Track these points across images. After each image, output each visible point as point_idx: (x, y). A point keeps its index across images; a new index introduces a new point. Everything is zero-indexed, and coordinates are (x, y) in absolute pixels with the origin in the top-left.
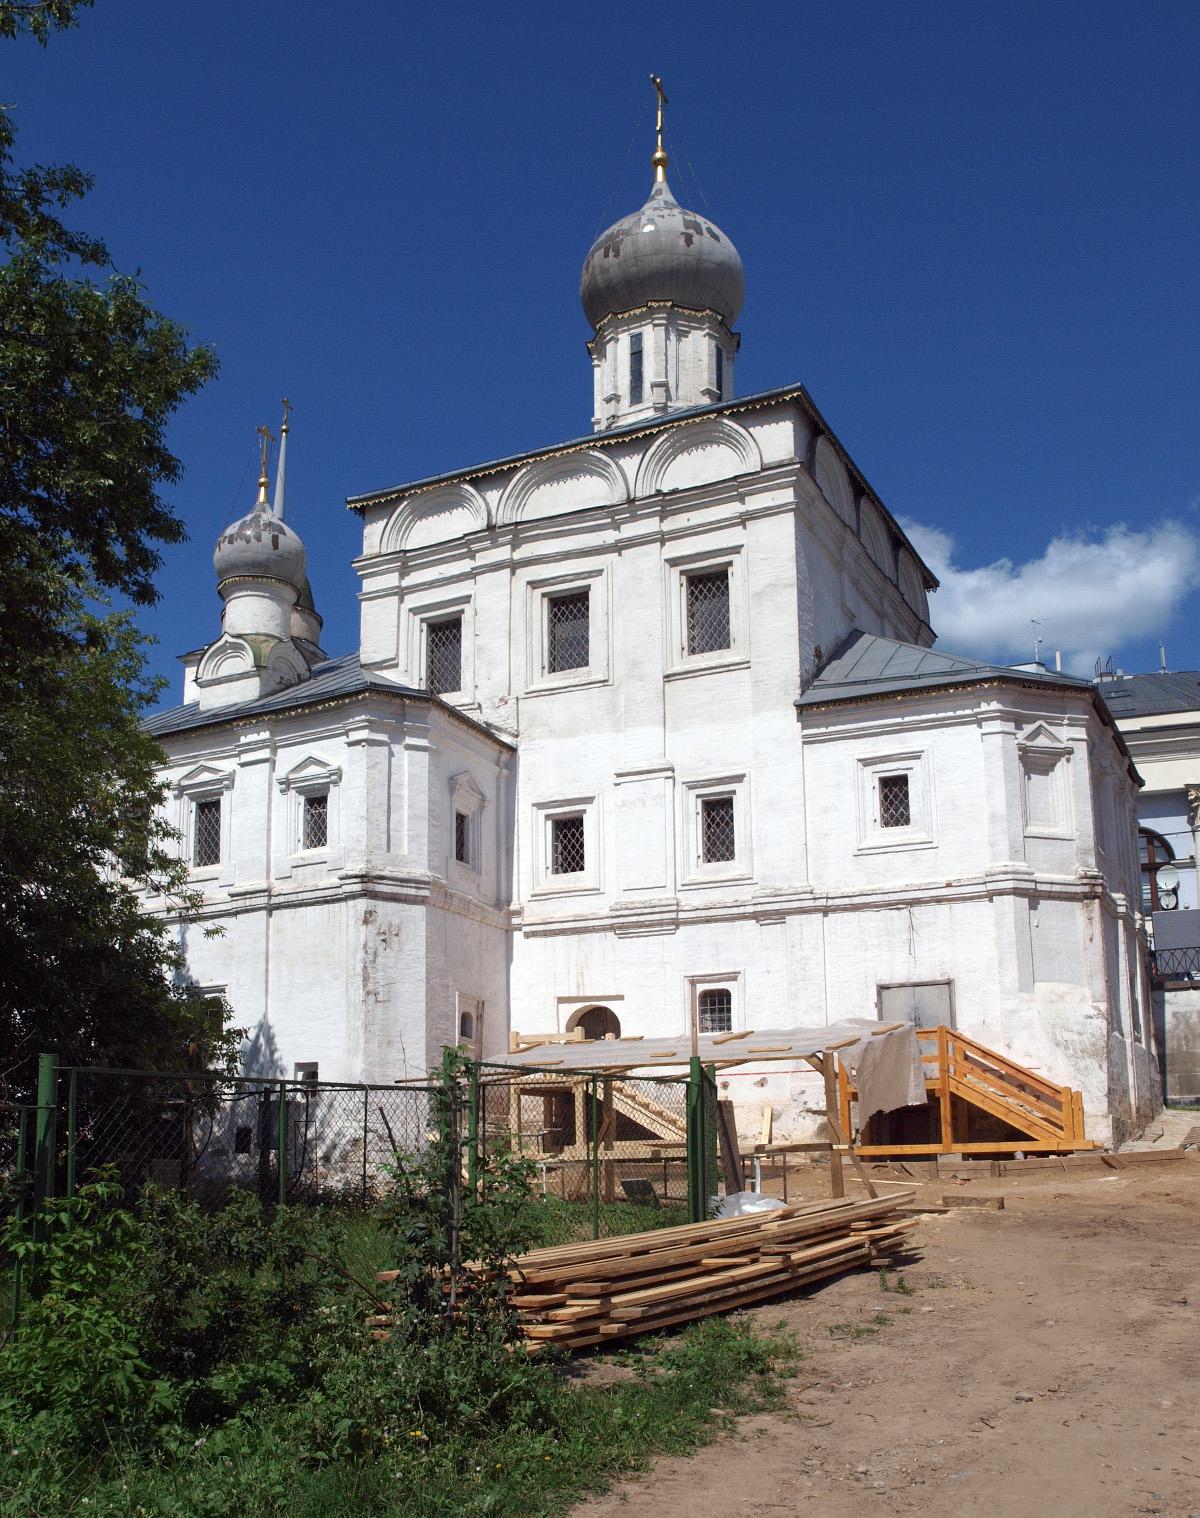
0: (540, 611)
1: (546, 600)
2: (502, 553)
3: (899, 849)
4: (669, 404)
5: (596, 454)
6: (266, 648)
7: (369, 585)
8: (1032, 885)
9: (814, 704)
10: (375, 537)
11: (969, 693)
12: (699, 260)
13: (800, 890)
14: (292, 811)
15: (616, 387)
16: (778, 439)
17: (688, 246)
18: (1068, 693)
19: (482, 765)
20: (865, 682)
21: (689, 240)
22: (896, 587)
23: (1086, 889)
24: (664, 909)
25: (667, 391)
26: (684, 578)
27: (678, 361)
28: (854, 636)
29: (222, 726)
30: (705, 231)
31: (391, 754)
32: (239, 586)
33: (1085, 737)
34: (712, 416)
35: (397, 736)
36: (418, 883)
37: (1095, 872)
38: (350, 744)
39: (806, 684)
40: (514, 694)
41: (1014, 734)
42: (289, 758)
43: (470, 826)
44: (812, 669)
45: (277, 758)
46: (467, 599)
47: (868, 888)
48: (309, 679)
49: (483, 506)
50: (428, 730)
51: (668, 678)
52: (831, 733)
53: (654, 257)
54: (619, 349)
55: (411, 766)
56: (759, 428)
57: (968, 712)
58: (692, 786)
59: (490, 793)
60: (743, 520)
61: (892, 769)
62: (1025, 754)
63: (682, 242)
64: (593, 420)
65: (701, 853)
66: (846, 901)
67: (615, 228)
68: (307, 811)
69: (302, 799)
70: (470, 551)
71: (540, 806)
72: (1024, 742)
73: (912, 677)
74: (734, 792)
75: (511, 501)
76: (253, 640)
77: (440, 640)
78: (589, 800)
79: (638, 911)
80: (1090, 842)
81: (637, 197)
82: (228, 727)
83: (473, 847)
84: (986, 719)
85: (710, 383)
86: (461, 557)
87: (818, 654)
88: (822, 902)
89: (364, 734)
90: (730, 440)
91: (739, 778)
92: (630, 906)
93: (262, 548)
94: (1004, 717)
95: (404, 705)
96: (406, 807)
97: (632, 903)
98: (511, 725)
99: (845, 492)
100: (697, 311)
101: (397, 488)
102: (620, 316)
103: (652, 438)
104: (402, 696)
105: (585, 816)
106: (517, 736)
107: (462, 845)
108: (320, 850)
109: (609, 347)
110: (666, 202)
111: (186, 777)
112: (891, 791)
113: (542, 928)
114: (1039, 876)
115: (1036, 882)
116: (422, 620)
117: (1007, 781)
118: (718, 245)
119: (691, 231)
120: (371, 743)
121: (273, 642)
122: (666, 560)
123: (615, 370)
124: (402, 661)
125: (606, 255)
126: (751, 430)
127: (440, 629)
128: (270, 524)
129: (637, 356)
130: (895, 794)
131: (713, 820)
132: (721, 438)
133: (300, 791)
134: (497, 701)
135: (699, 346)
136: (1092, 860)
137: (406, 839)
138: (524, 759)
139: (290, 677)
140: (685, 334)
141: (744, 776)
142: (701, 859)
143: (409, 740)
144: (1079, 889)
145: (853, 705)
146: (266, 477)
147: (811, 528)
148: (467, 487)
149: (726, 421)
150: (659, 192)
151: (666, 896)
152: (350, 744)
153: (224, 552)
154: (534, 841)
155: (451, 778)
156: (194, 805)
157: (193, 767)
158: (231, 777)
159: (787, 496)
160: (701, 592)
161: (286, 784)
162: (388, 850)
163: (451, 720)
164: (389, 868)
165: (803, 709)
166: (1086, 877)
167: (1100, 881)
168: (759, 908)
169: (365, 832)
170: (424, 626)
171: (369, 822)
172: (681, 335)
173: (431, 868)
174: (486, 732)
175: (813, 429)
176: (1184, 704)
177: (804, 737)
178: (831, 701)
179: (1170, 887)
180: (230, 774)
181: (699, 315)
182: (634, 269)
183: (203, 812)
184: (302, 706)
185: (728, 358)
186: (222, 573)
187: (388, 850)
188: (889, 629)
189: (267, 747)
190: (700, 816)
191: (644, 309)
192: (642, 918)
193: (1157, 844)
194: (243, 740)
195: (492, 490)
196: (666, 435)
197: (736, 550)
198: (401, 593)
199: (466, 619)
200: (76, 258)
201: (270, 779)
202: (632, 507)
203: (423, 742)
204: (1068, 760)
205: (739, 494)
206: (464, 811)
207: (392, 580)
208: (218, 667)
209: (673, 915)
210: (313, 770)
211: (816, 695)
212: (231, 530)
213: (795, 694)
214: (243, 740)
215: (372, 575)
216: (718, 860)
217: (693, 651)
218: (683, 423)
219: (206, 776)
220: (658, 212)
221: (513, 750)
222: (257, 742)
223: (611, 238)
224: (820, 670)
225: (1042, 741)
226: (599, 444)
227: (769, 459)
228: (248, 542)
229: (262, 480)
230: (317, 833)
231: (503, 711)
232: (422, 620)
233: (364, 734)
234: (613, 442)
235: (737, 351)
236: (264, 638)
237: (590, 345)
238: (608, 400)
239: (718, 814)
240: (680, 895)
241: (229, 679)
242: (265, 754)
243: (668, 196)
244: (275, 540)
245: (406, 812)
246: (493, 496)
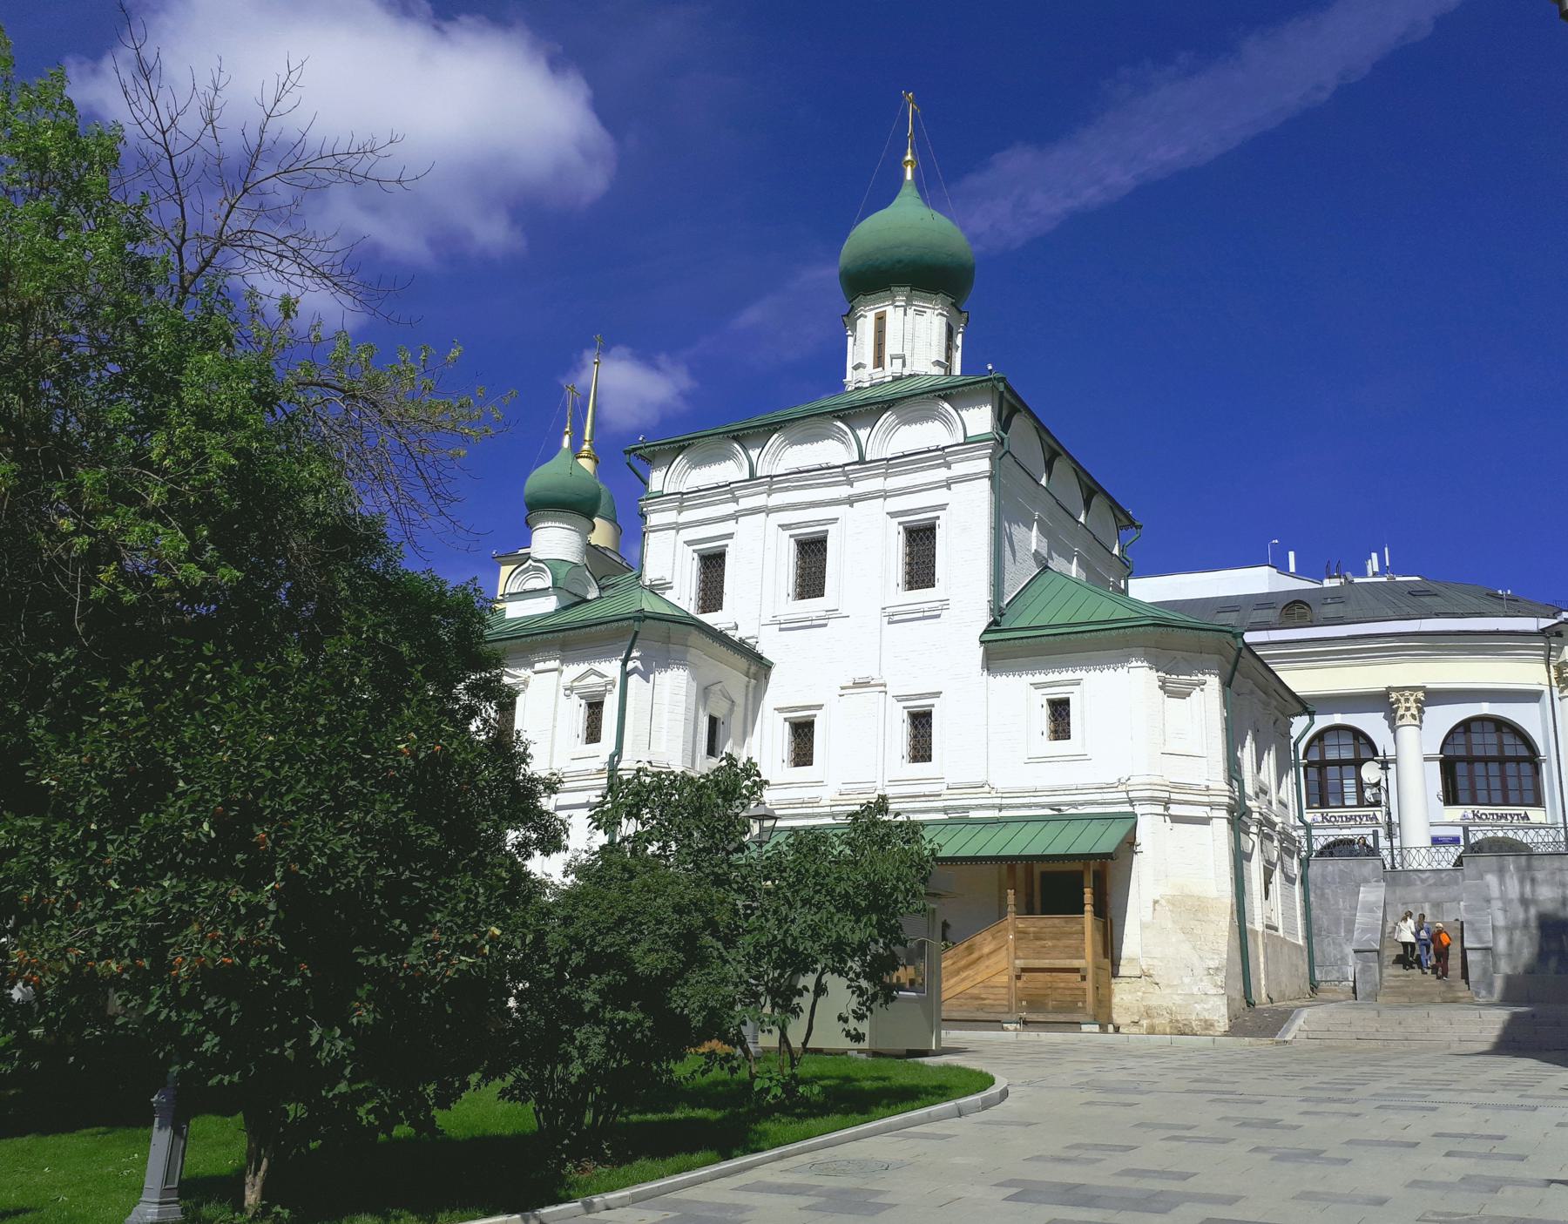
7: (654, 519)
14: (576, 714)
16: (980, 419)
19: (735, 679)
54: (866, 325)
58: (900, 699)
61: (1058, 693)
75: (768, 457)
76: (554, 565)
81: (886, 195)
91: (937, 694)
105: (816, 720)
126: (964, 413)
130: (1059, 711)
155: (706, 688)
158: (526, 683)
159: (984, 465)
176: (1390, 613)
179: (1374, 781)
190: (905, 724)
193: (1362, 741)
197: (943, 507)
201: (558, 685)
206: (716, 714)
239: (921, 722)
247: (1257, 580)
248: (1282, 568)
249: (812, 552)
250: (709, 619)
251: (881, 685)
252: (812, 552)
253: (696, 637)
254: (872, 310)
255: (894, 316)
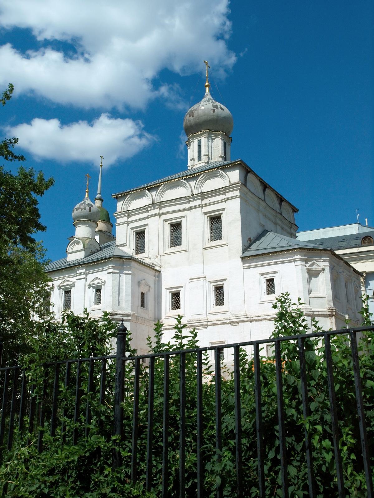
0: (168, 229)
1: (169, 225)
2: (156, 211)
3: (263, 302)
4: (209, 161)
5: (183, 181)
6: (87, 242)
7: (118, 221)
8: (312, 313)
9: (246, 257)
10: (120, 206)
11: (291, 253)
12: (217, 117)
13: (243, 315)
14: (91, 293)
15: (193, 156)
16: (235, 176)
17: (214, 113)
18: (322, 252)
19: (150, 277)
20: (262, 249)
21: (214, 111)
22: (281, 214)
23: (330, 313)
24: (203, 321)
25: (209, 157)
26: (209, 218)
27: (212, 147)
28: (264, 233)
29: (72, 268)
30: (219, 108)
31: (120, 276)
32: (79, 223)
33: (328, 265)
34: (216, 169)
35: (121, 271)
36: (127, 315)
37: (333, 307)
38: (108, 273)
39: (244, 251)
40: (160, 254)
41: (305, 265)
42: (90, 277)
43: (146, 296)
44: (247, 245)
45: (87, 278)
46: (146, 225)
47: (263, 314)
48: (100, 250)
49: (151, 197)
50: (131, 268)
51: (204, 249)
52: (251, 266)
53: (204, 117)
54: (194, 145)
55: (126, 279)
56: (229, 172)
57: (291, 258)
58: (211, 282)
59: (152, 285)
60: (225, 200)
61: (270, 276)
62: (309, 271)
63: (212, 112)
64: (188, 165)
65: (214, 303)
66: (256, 318)
67: (192, 108)
68: (96, 294)
69: (94, 290)
70: (147, 210)
71: (167, 289)
72: (308, 267)
73: (275, 248)
74: (224, 284)
75: (159, 195)
77: (139, 237)
78: (182, 287)
79: (196, 322)
80: (331, 298)
82: (73, 268)
83: (147, 304)
84: (296, 261)
85: (222, 154)
86: (145, 212)
87: (250, 239)
88: (249, 319)
89: (111, 270)
90: (221, 176)
91: (225, 280)
92: (193, 320)
93: (86, 211)
94: (302, 260)
95: (124, 261)
96: (124, 292)
97: (194, 319)
98: (159, 264)
99: (260, 188)
100: (217, 132)
101: (126, 191)
102: (194, 135)
103: (198, 176)
104: (123, 258)
105: (180, 292)
106: (161, 267)
107: (143, 302)
108: (99, 305)
109: (192, 144)
110: (209, 99)
111: (61, 283)
112: (270, 283)
113: (168, 327)
114: (314, 309)
115: (313, 312)
116: (134, 231)
117: (303, 280)
118: (224, 111)
119: (215, 108)
120: (114, 273)
121: (89, 240)
122: (203, 213)
123: (193, 151)
124: (128, 244)
125: (190, 117)
126: (227, 173)
127: (139, 234)
128: (88, 204)
129: (199, 146)
131: (218, 293)
132: (219, 176)
133: (94, 287)
134: (155, 256)
135: (218, 143)
136: (332, 304)
137: (124, 302)
138: (163, 274)
139: (95, 250)
140: (214, 139)
141: (226, 279)
142: (214, 305)
143: (125, 272)
144: (328, 313)
145: (257, 257)
146: (88, 189)
147: (246, 201)
148: (146, 191)
149: (220, 171)
150: (207, 95)
151: (204, 317)
152: (108, 273)
153: (75, 213)
154: (166, 300)
156: (64, 291)
157: (63, 280)
158: (74, 283)
159: (237, 193)
160: (214, 222)
161: (90, 285)
162: (119, 305)
163: (139, 264)
164: (119, 311)
165: (243, 258)
166: (330, 309)
167: (334, 311)
168: (231, 321)
169: (111, 300)
170: (135, 233)
171: (113, 297)
172: (213, 139)
173: (132, 310)
174: (151, 267)
175: (246, 171)
177: (243, 267)
178: (251, 256)
180: (74, 282)
181: (218, 133)
182: (198, 121)
183: (66, 294)
184: (94, 262)
185: (228, 145)
186: (74, 219)
187: (119, 305)
188: (279, 228)
189: (84, 274)
191: (201, 132)
192: (197, 324)
194: (78, 272)
195: (154, 191)
196: (203, 175)
197: (223, 209)
198: (128, 223)
199: (146, 231)
200: (17, 160)
201: (85, 284)
202: (193, 196)
203: (130, 272)
204: (323, 273)
205: (224, 192)
206: (143, 292)
207: (125, 219)
208: (73, 248)
209: (206, 323)
210: (97, 281)
211: (247, 254)
212: (77, 206)
213: (241, 253)
214: (78, 272)
215: (119, 218)
216: (220, 305)
217: (212, 240)
218: (207, 171)
219: (67, 283)
220: (205, 103)
221: (159, 272)
222: (81, 273)
223: (192, 111)
224: (250, 245)
225: (315, 267)
226: (183, 178)
227: (232, 182)
228: (82, 210)
229: (87, 190)
230: (98, 300)
231: (156, 259)
232: (134, 231)
233: (111, 270)
234: (187, 177)
235: (231, 142)
236: (86, 239)
237: (186, 143)
238: (191, 160)
239: (219, 290)
240: (208, 317)
241: (76, 252)
242: (84, 276)
243: (210, 97)
244: (90, 209)
245: (124, 293)
246: (154, 193)
247: (353, 229)
248: (362, 224)
249: (176, 227)
250: (140, 257)
251: (204, 277)
252: (176, 227)
253: (133, 263)
254: (196, 139)
255: (204, 140)
